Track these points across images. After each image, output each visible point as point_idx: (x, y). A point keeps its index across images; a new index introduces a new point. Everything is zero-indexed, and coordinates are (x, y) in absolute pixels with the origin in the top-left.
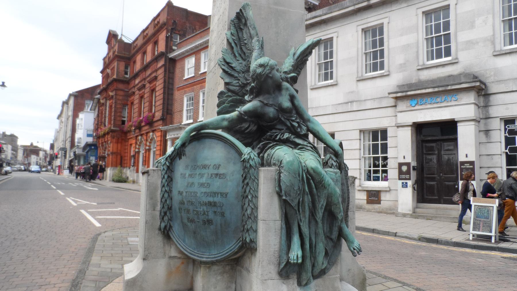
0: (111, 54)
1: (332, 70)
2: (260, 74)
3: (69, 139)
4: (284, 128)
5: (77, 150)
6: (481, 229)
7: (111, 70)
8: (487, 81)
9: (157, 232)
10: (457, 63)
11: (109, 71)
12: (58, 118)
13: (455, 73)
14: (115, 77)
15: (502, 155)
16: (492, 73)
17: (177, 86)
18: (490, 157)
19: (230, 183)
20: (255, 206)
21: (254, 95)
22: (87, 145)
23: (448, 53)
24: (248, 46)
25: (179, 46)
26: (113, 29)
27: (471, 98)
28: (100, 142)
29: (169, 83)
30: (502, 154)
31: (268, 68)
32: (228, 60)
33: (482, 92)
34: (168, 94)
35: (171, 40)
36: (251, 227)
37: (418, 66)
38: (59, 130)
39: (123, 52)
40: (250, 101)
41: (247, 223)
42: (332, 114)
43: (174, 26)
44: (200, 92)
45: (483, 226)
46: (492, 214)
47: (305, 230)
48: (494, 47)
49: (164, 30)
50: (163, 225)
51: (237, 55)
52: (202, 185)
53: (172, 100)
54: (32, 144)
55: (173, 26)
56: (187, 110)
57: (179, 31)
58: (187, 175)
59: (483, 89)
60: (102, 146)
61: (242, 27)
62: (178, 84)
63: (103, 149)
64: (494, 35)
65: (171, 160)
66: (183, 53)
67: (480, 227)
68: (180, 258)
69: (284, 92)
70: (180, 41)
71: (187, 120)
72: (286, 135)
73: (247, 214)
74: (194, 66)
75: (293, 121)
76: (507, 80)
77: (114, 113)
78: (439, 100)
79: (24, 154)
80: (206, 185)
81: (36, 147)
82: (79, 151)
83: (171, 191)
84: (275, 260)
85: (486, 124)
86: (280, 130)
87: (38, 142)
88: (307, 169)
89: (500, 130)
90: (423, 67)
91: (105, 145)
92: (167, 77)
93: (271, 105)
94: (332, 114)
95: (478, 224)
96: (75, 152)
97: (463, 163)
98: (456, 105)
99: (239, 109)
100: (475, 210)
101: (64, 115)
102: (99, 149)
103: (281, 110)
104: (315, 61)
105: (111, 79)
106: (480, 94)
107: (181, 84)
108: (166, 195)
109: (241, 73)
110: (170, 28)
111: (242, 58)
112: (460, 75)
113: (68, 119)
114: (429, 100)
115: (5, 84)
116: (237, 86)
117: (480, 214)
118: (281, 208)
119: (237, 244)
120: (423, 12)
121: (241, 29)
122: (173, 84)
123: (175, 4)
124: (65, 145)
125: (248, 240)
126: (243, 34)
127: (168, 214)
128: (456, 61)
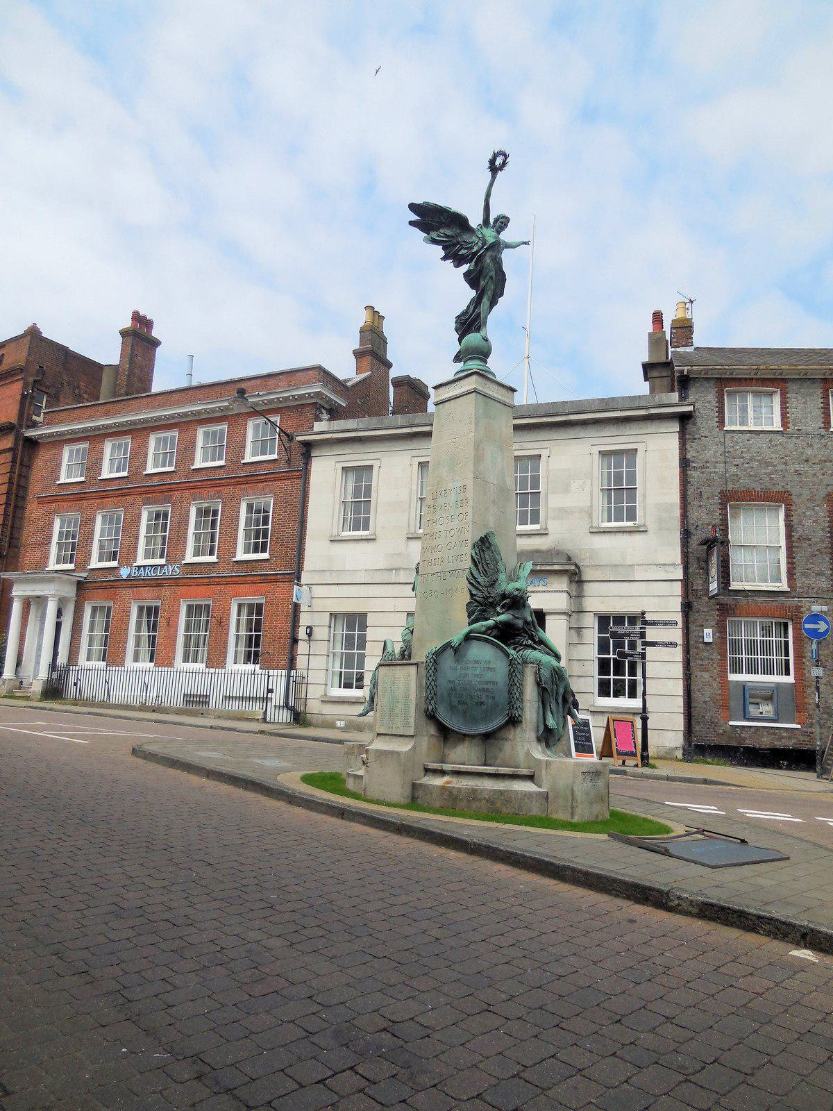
8: (582, 564)
13: (544, 548)
16: (588, 555)
19: (499, 675)
27: (562, 584)
40: (502, 614)
43: (41, 376)
49: (17, 380)
50: (430, 708)
52: (477, 676)
53: (22, 519)
62: (36, 487)
66: (61, 434)
68: (436, 736)
69: (527, 609)
70: (47, 411)
71: (58, 562)
85: (578, 620)
92: (17, 473)
98: (544, 592)
110: (31, 379)
122: (25, 488)
123: (46, 334)
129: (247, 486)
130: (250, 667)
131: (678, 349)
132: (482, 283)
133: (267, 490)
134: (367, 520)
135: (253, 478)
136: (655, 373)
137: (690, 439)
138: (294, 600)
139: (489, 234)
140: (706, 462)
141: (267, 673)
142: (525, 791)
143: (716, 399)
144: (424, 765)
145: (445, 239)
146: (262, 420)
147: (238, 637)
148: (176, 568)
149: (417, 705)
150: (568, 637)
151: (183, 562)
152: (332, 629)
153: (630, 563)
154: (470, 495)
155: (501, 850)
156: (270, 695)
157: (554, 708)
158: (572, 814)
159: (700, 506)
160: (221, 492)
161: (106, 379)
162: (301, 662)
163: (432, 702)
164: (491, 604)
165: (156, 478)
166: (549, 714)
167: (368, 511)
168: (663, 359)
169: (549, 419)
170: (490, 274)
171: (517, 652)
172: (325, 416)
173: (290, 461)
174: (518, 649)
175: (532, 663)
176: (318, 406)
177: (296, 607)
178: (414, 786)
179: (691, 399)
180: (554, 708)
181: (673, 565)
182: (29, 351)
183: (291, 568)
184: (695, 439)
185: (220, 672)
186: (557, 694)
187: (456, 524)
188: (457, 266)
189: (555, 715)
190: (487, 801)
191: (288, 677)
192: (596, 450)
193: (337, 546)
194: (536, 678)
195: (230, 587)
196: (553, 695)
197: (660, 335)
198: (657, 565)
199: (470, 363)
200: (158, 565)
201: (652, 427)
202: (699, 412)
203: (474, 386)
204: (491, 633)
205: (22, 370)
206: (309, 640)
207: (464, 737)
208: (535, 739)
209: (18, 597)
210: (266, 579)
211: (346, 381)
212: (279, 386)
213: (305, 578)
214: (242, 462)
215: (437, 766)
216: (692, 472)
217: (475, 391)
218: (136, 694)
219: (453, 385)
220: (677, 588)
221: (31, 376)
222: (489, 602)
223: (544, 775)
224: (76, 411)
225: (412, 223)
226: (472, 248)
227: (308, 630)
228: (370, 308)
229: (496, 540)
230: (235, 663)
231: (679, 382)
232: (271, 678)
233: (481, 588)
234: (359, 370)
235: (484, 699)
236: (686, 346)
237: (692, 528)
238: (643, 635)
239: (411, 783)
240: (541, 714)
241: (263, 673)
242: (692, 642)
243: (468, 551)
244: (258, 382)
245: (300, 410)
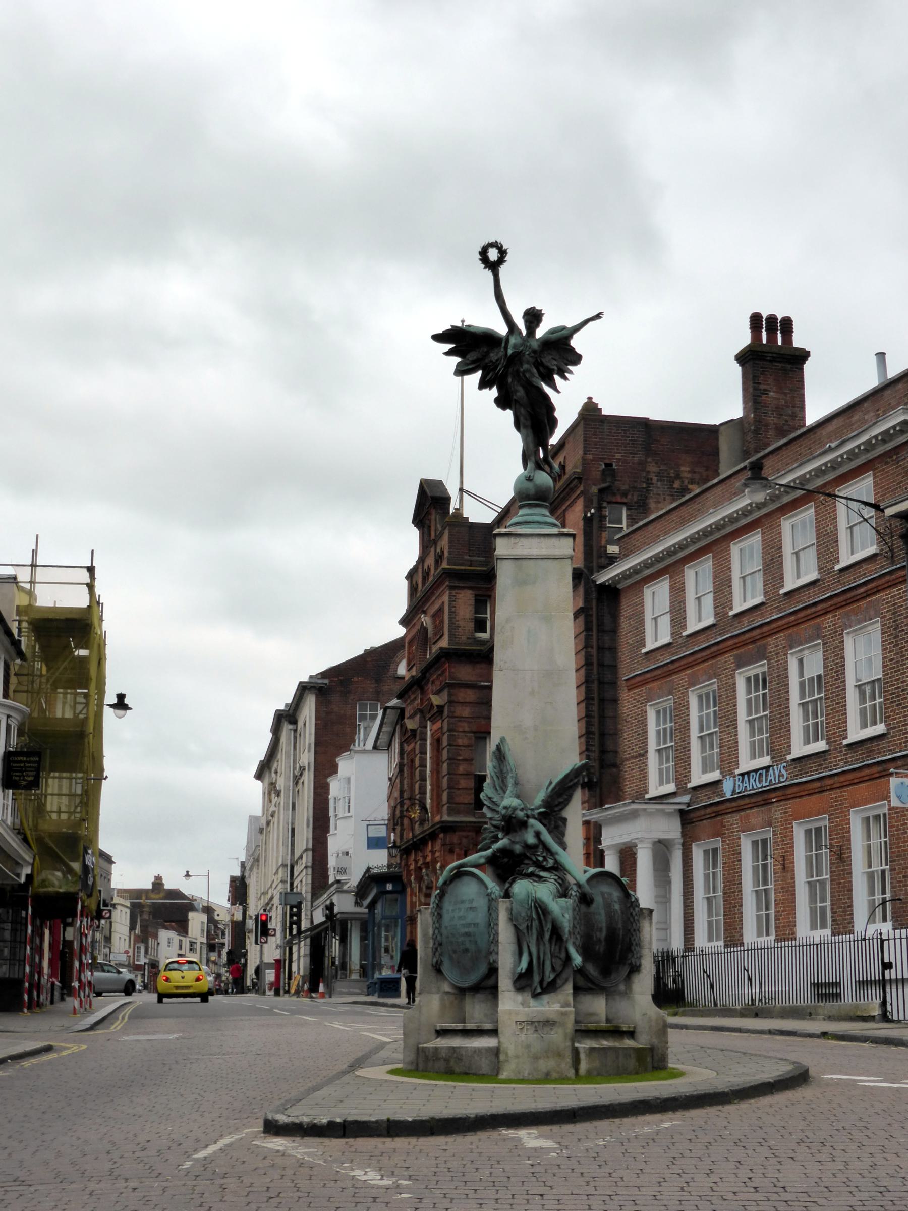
0: (430, 561)
1: (704, 755)
3: (307, 859)
4: (530, 862)
5: (335, 899)
7: (434, 616)
11: (426, 620)
12: (259, 776)
14: (444, 643)
17: (625, 674)
22: (371, 880)
25: (628, 544)
26: (432, 475)
28: (412, 867)
29: (601, 665)
32: (490, 795)
34: (602, 701)
35: (602, 528)
38: (263, 822)
39: (467, 557)
43: (609, 479)
44: (690, 693)
47: (534, 950)
49: (578, 497)
50: (435, 960)
51: (498, 788)
52: (460, 918)
53: (616, 717)
54: (158, 883)
55: (604, 481)
56: (701, 738)
57: (625, 495)
60: (419, 879)
62: (629, 668)
63: (420, 889)
66: (635, 571)
68: (454, 994)
70: (631, 529)
72: (531, 869)
74: (668, 610)
75: (538, 855)
77: (449, 765)
79: (132, 928)
81: (176, 894)
82: (344, 904)
83: (440, 926)
84: (510, 975)
86: (527, 864)
87: (188, 875)
91: (427, 875)
93: (517, 843)
96: (330, 907)
101: (282, 763)
102: (409, 890)
103: (527, 846)
105: (435, 649)
107: (634, 671)
108: (437, 932)
110: (594, 490)
113: (297, 780)
115: (126, 701)
122: (614, 668)
123: (608, 410)
124: (292, 884)
125: (491, 961)
127: (439, 949)
129: (848, 608)
133: (872, 612)
142: (475, 1047)
148: (782, 770)
151: (789, 758)
160: (819, 628)
161: (726, 447)
165: (745, 620)
182: (584, 450)
195: (846, 793)
200: (762, 769)
205: (580, 479)
209: (609, 847)
218: (780, 989)
221: (595, 485)
224: (650, 528)
232: (886, 943)
235: (468, 945)
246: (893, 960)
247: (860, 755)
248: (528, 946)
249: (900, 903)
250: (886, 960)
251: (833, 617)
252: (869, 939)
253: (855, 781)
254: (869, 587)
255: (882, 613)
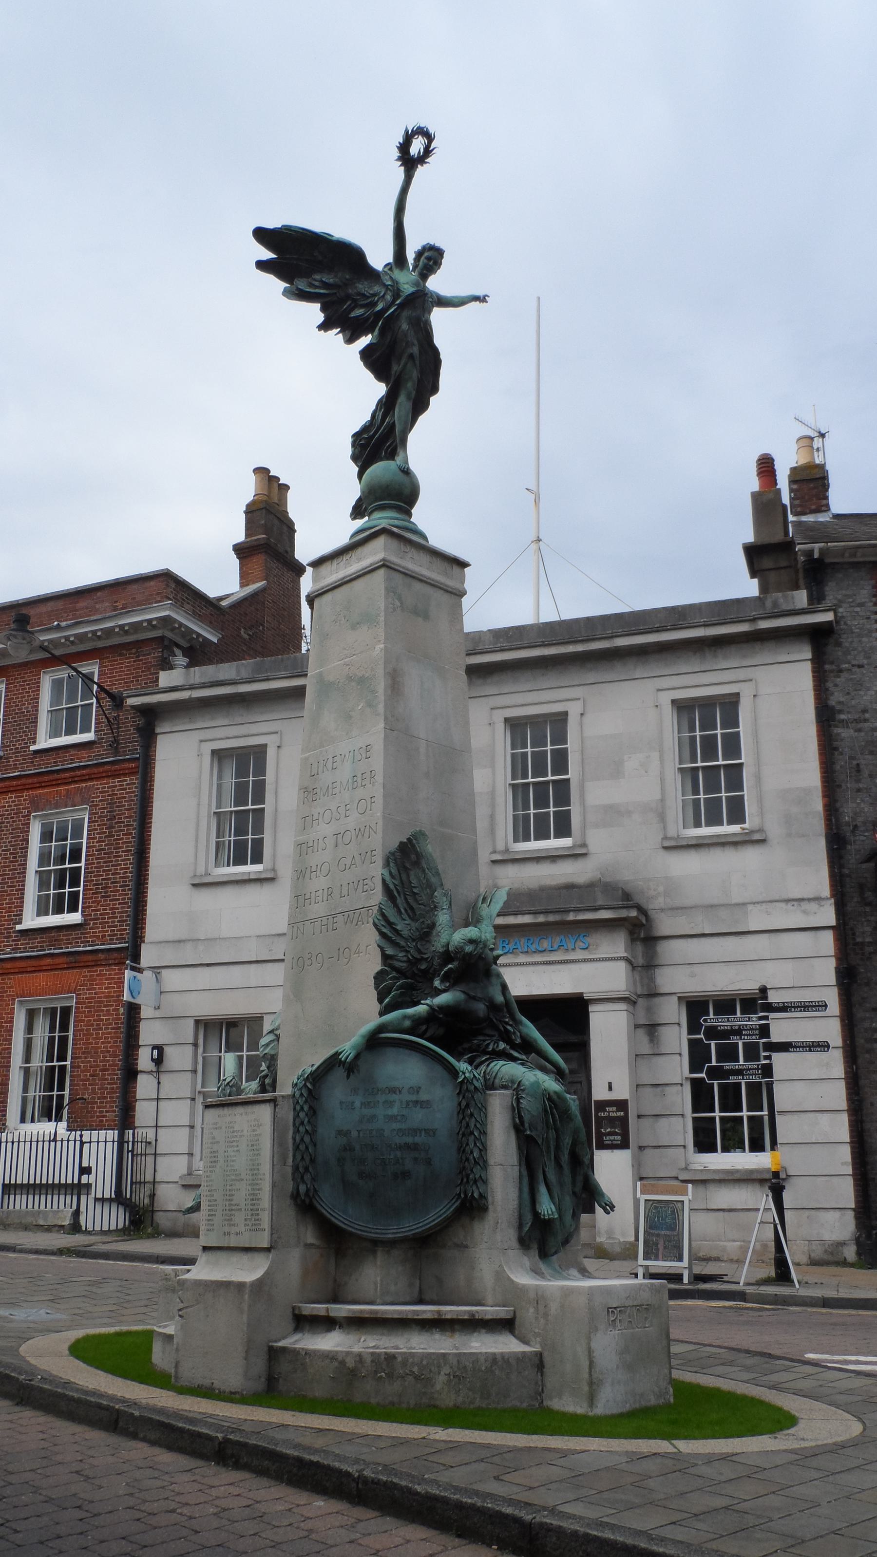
2: (470, 954)
4: (496, 1033)
6: (660, 1256)
8: (651, 907)
9: (289, 1201)
10: (585, 855)
13: (581, 879)
15: (684, 1086)
16: (661, 889)
18: (659, 1089)
20: (484, 1147)
21: (452, 981)
23: (563, 828)
24: (420, 898)
30: (684, 1082)
31: (481, 946)
33: (639, 933)
36: (480, 1176)
37: (494, 852)
40: (444, 991)
41: (474, 1170)
42: (257, 962)
45: (665, 1248)
46: (681, 1218)
48: (665, 828)
50: (302, 1188)
51: (403, 911)
52: (393, 1118)
58: (357, 1104)
59: (643, 925)
61: (408, 865)
64: (662, 800)
65: (313, 1080)
67: (658, 1250)
68: (318, 1247)
69: (494, 980)
73: (474, 1157)
76: (691, 908)
78: (546, 944)
80: (399, 1118)
83: (315, 1131)
85: (649, 1010)
88: (549, 1094)
89: (679, 1024)
90: (506, 857)
94: (257, 962)
95: (654, 1244)
97: (602, 1105)
98: (585, 961)
99: (428, 1002)
100: (647, 1211)
103: (493, 1007)
104: (210, 805)
106: (636, 936)
109: (410, 940)
111: (409, 916)
112: (591, 886)
114: (522, 943)
116: (404, 962)
117: (656, 1219)
118: (520, 1148)
119: (453, 1205)
120: (507, 720)
121: (406, 869)
126: (408, 876)
128: (583, 851)
130: (47, 1128)
131: (804, 518)
132: (395, 368)
134: (258, 845)
135: (51, 777)
136: (767, 563)
137: (832, 671)
138: (126, 997)
139: (406, 280)
140: (864, 711)
141: (78, 1138)
142: (494, 1354)
143: (874, 599)
144: (294, 1308)
145: (322, 291)
146: (63, 673)
147: (27, 1072)
149: (274, 1185)
150: (632, 1040)
152: (200, 1050)
153: (740, 901)
154: (378, 763)
155: (418, 1494)
156: (85, 1179)
157: (552, 1176)
158: (591, 1399)
159: (859, 790)
162: (144, 1112)
163: (307, 1177)
164: (425, 972)
166: (543, 1190)
167: (259, 828)
168: (779, 537)
169: (580, 648)
170: (410, 351)
171: (476, 1068)
172: (180, 660)
173: (118, 744)
174: (478, 1061)
175: (505, 1087)
176: (166, 643)
177: (133, 1010)
178: (274, 1354)
179: (829, 602)
180: (552, 1176)
181: (817, 899)
183: (121, 940)
184: (841, 671)
185: (102, 1139)
186: (558, 1148)
187: (352, 821)
188: (350, 340)
189: (556, 1191)
190: (417, 1378)
191: (121, 1142)
192: (666, 699)
193: (205, 897)
194: (513, 1118)
196: (548, 1152)
197: (771, 496)
198: (788, 901)
199: (377, 515)
201: (764, 655)
202: (845, 624)
203: (380, 556)
204: (426, 1031)
206: (158, 1072)
207: (375, 1244)
208: (514, 1243)
210: (76, 961)
211: (221, 599)
212: (95, 611)
213: (148, 956)
214: (33, 748)
215: (320, 1308)
216: (840, 730)
217: (385, 565)
219: (345, 557)
220: (827, 942)
222: (420, 970)
223: (528, 1316)
225: (262, 265)
226: (375, 304)
227: (155, 1052)
228: (262, 472)
229: (431, 848)
230: (23, 1120)
231: (806, 571)
232: (86, 1146)
233: (403, 943)
234: (245, 579)
236: (818, 510)
237: (847, 830)
238: (764, 1031)
239: (266, 1349)
240: (526, 1189)
241: (72, 1138)
242: (860, 1041)
243: (377, 871)
244: (60, 604)
245: (134, 651)
246: (93, 1165)
247: (38, 942)
248: (544, 1172)
249: (82, 1103)
250: (85, 1164)
251: (15, 797)
252: (62, 1141)
253: (29, 969)
254: (78, 773)
255: (93, 802)
